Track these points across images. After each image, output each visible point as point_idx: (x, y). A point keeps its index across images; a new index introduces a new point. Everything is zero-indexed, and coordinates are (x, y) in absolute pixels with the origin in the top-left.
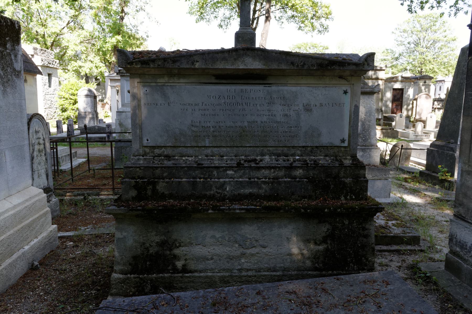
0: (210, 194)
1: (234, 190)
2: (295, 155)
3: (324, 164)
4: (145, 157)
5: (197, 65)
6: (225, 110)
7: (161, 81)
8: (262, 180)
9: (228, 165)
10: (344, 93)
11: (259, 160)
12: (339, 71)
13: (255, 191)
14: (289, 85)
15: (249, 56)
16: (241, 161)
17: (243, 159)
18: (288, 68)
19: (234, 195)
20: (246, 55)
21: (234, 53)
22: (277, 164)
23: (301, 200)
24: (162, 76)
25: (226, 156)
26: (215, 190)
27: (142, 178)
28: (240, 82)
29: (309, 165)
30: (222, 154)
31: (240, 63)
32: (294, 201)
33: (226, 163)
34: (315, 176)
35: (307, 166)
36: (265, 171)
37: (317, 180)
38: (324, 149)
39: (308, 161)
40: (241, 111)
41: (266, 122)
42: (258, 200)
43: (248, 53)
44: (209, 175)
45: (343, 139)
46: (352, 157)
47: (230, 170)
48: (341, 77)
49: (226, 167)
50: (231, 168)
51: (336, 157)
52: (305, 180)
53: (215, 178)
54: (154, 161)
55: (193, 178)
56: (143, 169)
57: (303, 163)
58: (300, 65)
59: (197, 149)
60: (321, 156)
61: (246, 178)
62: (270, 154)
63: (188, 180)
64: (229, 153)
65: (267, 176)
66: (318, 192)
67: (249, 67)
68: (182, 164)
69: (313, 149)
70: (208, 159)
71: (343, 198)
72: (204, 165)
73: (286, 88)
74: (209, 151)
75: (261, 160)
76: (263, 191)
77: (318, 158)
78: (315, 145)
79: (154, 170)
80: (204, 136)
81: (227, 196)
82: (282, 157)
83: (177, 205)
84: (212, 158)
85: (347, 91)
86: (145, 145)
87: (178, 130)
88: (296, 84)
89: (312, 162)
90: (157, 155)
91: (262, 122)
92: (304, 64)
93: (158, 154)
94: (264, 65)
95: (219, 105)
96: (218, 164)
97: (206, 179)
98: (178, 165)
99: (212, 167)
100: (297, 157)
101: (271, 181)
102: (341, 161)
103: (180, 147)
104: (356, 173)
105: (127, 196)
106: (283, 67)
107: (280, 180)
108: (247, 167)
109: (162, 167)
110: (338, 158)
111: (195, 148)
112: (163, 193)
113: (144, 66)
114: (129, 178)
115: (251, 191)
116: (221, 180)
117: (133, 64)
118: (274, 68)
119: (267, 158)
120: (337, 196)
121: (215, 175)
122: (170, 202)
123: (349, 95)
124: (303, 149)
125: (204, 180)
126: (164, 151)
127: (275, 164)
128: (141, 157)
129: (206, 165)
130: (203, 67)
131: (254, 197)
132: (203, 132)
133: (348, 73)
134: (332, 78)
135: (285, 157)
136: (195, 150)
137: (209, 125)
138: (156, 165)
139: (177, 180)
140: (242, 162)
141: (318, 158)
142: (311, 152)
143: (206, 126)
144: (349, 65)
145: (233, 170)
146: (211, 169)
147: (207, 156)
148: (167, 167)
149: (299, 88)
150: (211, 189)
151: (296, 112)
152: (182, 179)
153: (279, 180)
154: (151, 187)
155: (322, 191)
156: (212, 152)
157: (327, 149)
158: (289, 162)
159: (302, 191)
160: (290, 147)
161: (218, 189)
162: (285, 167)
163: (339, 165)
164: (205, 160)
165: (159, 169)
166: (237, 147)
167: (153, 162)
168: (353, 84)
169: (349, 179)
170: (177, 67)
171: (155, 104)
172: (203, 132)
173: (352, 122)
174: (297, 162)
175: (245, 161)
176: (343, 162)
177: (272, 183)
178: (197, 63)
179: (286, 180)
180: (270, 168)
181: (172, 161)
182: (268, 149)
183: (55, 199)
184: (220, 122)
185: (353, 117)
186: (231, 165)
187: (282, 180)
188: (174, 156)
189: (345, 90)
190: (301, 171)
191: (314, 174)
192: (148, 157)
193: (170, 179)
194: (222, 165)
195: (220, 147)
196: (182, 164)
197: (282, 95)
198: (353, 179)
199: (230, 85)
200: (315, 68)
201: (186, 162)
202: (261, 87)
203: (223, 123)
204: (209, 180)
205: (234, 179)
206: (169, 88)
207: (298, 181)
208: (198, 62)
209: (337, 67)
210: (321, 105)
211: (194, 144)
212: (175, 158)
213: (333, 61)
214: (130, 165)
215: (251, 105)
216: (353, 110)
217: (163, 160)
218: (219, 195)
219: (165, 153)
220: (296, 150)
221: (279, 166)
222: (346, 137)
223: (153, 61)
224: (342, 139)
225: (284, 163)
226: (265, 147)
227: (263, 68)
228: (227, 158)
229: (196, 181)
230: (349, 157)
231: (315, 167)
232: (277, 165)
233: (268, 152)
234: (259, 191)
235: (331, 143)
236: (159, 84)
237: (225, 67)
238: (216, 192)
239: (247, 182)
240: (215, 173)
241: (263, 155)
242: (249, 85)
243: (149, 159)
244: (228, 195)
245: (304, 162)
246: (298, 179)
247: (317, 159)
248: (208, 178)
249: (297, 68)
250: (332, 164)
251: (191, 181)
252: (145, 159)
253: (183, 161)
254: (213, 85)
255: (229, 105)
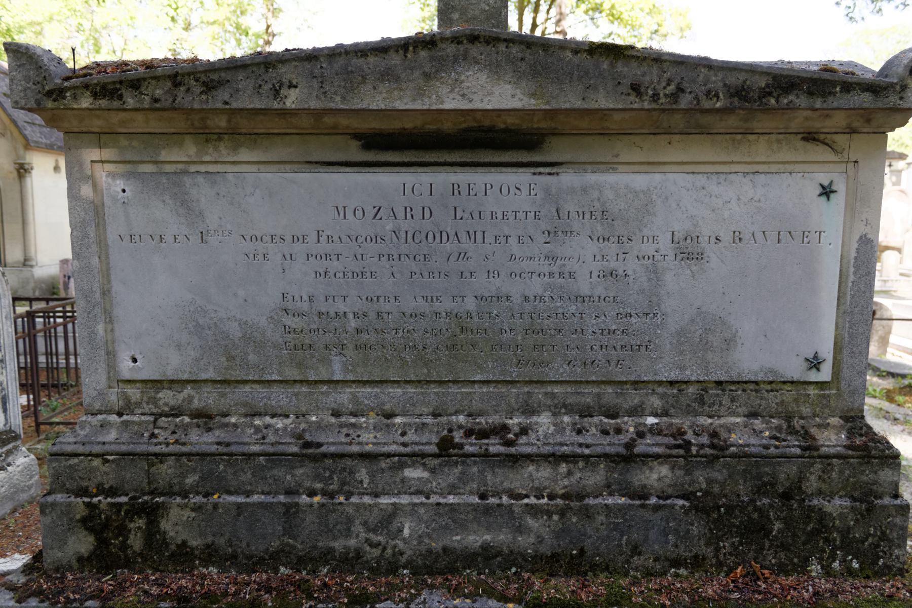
0: (345, 547)
1: (429, 536)
2: (643, 410)
3: (748, 445)
4: (125, 417)
5: (292, 99)
6: (396, 257)
7: (173, 155)
8: (526, 501)
9: (408, 450)
10: (820, 195)
11: (516, 429)
12: (809, 113)
13: (501, 538)
14: (621, 168)
15: (477, 63)
16: (455, 434)
17: (460, 427)
18: (620, 106)
19: (430, 551)
20: (465, 59)
21: (423, 53)
22: (581, 445)
23: (664, 574)
24: (174, 138)
25: (404, 415)
26: (363, 535)
27: (112, 492)
28: (449, 160)
29: (694, 450)
30: (387, 407)
31: (444, 90)
32: (639, 575)
33: (402, 439)
34: (716, 489)
35: (688, 455)
36: (538, 471)
37: (723, 505)
38: (744, 390)
39: (690, 436)
40: (452, 259)
41: (541, 299)
42: (514, 570)
43: (475, 50)
44: (343, 483)
45: (816, 357)
46: (846, 419)
47: (413, 465)
48: (810, 137)
49: (401, 455)
50: (417, 457)
51: (789, 418)
52: (681, 502)
53: (363, 494)
54: (156, 431)
55: (288, 492)
56: (113, 461)
57: (672, 441)
58: (666, 95)
59: (304, 389)
60: (734, 414)
61: (471, 493)
62: (556, 406)
63: (269, 499)
64: (414, 405)
65: (545, 488)
66: (726, 545)
67: (477, 105)
68: (248, 444)
69: (705, 390)
70: (341, 426)
71: (815, 568)
72: (324, 449)
73: (610, 178)
74: (343, 397)
75: (524, 431)
76: (532, 539)
77: (723, 421)
78: (715, 378)
79: (152, 465)
80: (326, 347)
81: (405, 556)
82: (596, 420)
83: (225, 594)
84: (353, 420)
85: (834, 188)
86: (127, 375)
87: (236, 324)
88: (649, 163)
89: (705, 440)
90: (167, 409)
91: (526, 299)
92: (680, 90)
93: (173, 408)
94: (533, 95)
95: (375, 239)
96: (374, 444)
97: (332, 495)
98: (233, 449)
99: (351, 456)
100: (651, 420)
101: (557, 506)
102: (807, 435)
103: (245, 382)
104: (865, 478)
105: (60, 554)
106: (602, 101)
107: (591, 501)
108: (474, 455)
109: (179, 455)
110: (797, 423)
111: (298, 386)
112: (184, 543)
113: (103, 103)
114: (68, 492)
115: (488, 537)
116: (384, 500)
117: (64, 98)
118: (568, 106)
119: (544, 420)
120: (796, 560)
121: (361, 482)
122: (203, 577)
123: (839, 200)
124: (669, 392)
125: (324, 501)
126: (190, 399)
127: (572, 444)
128: (114, 418)
129: (333, 449)
130: (314, 104)
131: (499, 559)
132: (321, 332)
133: (839, 120)
134: (779, 142)
135: (607, 417)
136: (297, 394)
137: (341, 307)
138: (157, 449)
139: (232, 499)
140: (458, 437)
141: (723, 421)
142: (701, 401)
143: (332, 314)
144: (848, 91)
145: (424, 465)
146: (349, 462)
147: (336, 414)
148: (198, 454)
149: (658, 177)
150: (348, 533)
151: (646, 262)
152: (248, 494)
153: (587, 501)
154: (141, 522)
155: (741, 544)
156: (354, 398)
157: (756, 391)
158: (621, 437)
159: (667, 542)
160: (626, 383)
161: (374, 531)
162: (606, 456)
163: (804, 449)
164: (329, 426)
165: (171, 461)
166: (441, 383)
167: (153, 435)
168: (856, 162)
169: (837, 502)
170: (219, 105)
171: (157, 238)
172: (321, 332)
173: (849, 297)
174: (649, 436)
175: (469, 433)
176: (814, 439)
177: (562, 513)
178: (292, 90)
179: (610, 501)
180: (554, 459)
181: (217, 433)
182: (549, 389)
183: (27, 459)
184: (382, 299)
185: (852, 278)
186: (417, 448)
187: (597, 501)
188: (225, 415)
189: (826, 183)
190: (665, 470)
191: (710, 481)
192: (136, 418)
193: (207, 495)
194: (386, 449)
195: (382, 382)
196: (248, 444)
197: (597, 205)
198: (854, 499)
199: (412, 169)
200: (718, 105)
201: (264, 438)
202: (523, 177)
203: (392, 300)
204: (342, 499)
205: (428, 498)
206: (200, 179)
207: (655, 505)
208: (296, 87)
209: (802, 101)
210: (738, 237)
211: (292, 373)
212: (227, 420)
213: (787, 76)
214: (69, 449)
215: (489, 239)
216: (853, 254)
217: (186, 428)
218: (376, 552)
219: (196, 404)
220: (647, 394)
221: (587, 451)
222: (827, 351)
223: (135, 84)
224: (810, 356)
225: (607, 440)
226: (537, 382)
227: (527, 107)
228: (405, 420)
229: (297, 504)
230: (835, 421)
231: (717, 457)
232: (579, 450)
233: (549, 402)
234: (514, 538)
235: (772, 371)
236: (169, 168)
237: (390, 106)
238: (367, 540)
239: (475, 508)
240: (363, 474)
241: (530, 410)
242: (479, 169)
243: (140, 424)
244: (409, 553)
245: (673, 436)
246: (653, 500)
247: (721, 426)
248: (339, 492)
249: (654, 106)
250: (777, 447)
251: (280, 503)
252: (126, 424)
253: (256, 433)
254: (356, 169)
255: (410, 239)
